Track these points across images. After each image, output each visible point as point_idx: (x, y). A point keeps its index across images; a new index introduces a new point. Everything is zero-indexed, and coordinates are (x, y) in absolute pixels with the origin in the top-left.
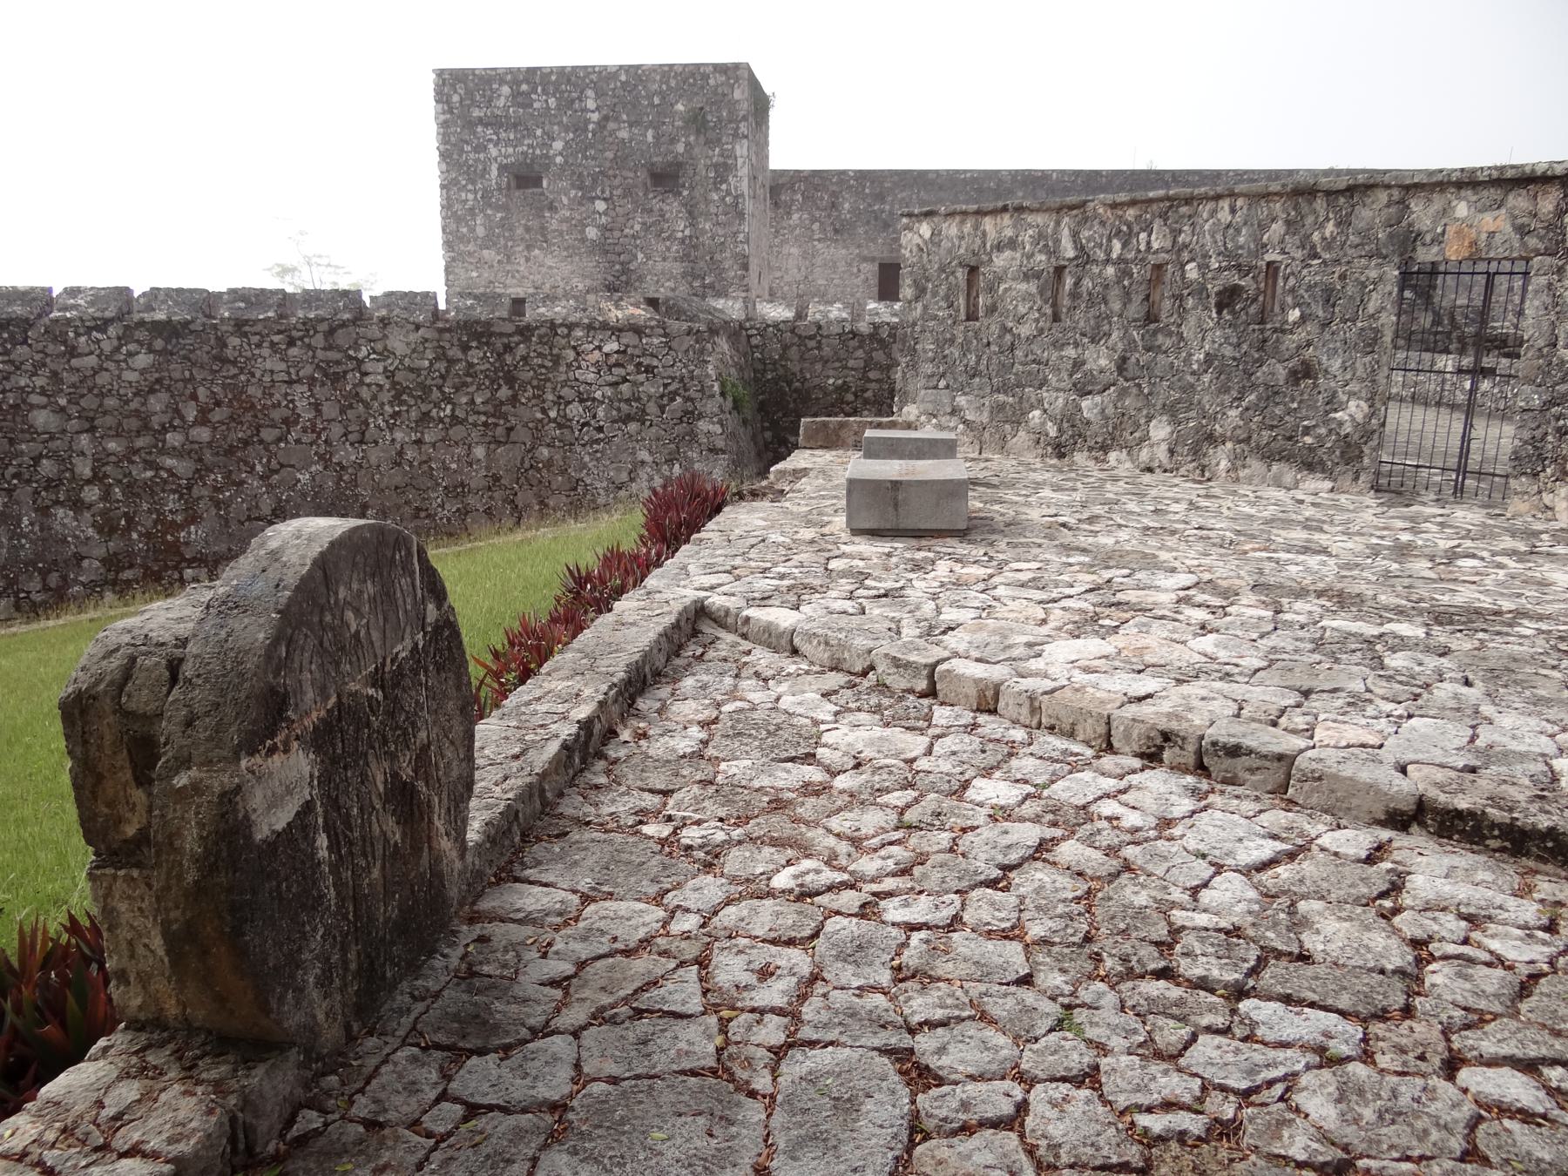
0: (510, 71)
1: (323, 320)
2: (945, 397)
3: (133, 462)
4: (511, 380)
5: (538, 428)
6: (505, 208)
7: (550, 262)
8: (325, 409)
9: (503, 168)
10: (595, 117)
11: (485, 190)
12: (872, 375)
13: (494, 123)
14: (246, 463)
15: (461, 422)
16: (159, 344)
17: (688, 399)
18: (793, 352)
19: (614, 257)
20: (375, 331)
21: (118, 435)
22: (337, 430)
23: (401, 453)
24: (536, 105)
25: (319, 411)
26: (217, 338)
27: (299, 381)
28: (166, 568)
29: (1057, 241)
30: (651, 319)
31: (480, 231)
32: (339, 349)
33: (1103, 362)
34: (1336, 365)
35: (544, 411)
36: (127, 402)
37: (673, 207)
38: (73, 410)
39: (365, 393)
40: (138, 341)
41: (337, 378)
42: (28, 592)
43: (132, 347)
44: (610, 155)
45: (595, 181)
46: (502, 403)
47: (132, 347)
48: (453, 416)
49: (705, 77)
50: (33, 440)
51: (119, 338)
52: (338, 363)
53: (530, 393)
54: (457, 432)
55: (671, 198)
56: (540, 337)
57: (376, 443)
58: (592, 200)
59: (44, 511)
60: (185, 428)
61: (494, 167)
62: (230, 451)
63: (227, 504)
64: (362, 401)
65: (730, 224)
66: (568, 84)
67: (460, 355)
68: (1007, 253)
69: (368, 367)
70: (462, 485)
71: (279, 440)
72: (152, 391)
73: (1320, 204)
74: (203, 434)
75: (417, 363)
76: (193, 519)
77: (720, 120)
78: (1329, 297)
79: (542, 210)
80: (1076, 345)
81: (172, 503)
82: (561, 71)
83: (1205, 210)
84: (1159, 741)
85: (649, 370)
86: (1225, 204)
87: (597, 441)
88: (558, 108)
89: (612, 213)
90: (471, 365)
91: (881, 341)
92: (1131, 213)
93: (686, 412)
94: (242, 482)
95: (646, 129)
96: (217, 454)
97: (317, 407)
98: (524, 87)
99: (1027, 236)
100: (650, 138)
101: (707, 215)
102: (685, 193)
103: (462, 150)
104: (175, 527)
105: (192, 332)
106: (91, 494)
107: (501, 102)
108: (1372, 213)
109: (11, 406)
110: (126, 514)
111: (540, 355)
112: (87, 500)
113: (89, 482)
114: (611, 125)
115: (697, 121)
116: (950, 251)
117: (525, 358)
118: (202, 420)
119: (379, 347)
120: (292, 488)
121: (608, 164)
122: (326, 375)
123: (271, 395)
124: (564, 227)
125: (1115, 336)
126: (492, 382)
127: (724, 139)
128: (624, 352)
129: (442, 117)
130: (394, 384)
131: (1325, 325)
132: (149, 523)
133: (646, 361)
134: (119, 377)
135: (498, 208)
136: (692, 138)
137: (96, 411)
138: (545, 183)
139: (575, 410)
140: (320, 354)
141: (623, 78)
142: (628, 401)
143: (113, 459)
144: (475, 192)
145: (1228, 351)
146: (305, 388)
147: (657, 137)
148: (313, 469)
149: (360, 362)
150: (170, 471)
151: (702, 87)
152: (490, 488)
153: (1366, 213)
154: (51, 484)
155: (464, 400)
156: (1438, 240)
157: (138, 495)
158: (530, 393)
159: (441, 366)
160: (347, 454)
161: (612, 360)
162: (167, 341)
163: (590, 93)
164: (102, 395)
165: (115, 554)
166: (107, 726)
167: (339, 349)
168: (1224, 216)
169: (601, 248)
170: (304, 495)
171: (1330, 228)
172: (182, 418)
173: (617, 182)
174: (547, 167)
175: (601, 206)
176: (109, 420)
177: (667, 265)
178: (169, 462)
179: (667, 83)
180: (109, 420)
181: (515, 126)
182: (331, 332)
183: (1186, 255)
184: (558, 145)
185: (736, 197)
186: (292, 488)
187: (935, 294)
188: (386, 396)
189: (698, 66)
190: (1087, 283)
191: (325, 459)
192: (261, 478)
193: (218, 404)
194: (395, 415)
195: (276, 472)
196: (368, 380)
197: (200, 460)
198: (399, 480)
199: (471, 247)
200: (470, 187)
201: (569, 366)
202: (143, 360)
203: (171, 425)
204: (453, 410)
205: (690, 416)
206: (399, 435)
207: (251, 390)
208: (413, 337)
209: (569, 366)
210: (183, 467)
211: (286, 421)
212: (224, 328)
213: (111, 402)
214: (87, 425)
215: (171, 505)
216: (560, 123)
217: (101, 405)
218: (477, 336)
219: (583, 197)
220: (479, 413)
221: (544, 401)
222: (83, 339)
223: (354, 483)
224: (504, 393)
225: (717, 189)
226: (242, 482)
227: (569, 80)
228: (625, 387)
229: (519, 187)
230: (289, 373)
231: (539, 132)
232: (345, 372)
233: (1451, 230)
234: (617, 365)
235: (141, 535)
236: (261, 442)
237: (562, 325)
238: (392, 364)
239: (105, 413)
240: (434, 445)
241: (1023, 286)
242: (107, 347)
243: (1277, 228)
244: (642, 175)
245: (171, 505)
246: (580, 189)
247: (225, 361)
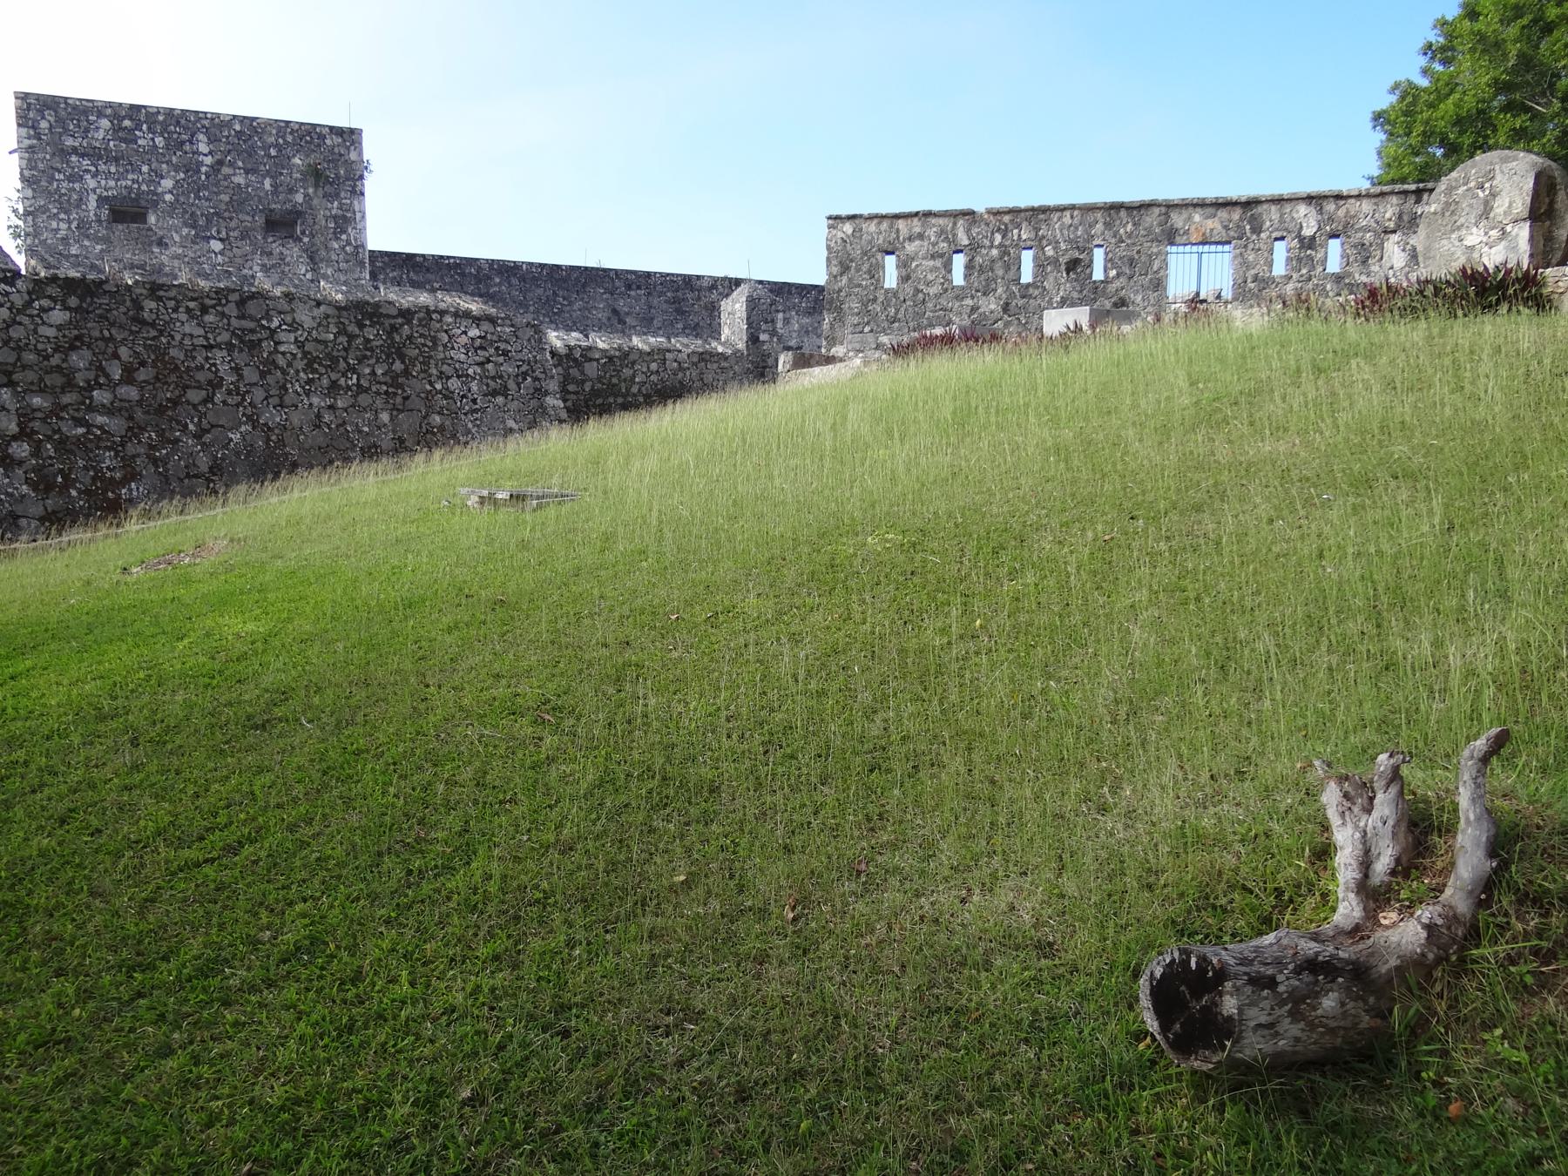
0: (110, 105)
1: (234, 291)
2: (870, 338)
3: (62, 419)
4: (402, 357)
5: (429, 396)
6: (106, 240)
8: (246, 372)
9: (102, 200)
10: (208, 160)
12: (571, 388)
13: (93, 154)
14: (178, 422)
15: (367, 390)
16: (73, 301)
17: (536, 379)
21: (41, 391)
22: (259, 394)
23: (319, 416)
25: (241, 377)
27: (218, 346)
29: (955, 235)
32: (252, 318)
33: (993, 307)
34: (1139, 298)
35: (431, 383)
36: (47, 358)
37: (293, 252)
39: (281, 362)
40: (50, 297)
41: (254, 346)
43: (45, 303)
44: (225, 198)
45: (209, 221)
46: (398, 376)
48: (358, 385)
49: (322, 137)
51: (29, 293)
52: (252, 331)
53: (418, 368)
54: (364, 400)
55: (291, 244)
56: (420, 320)
60: (112, 386)
61: (93, 199)
62: (161, 410)
63: (165, 461)
65: (353, 271)
66: (179, 126)
67: (357, 331)
68: (917, 242)
69: (282, 336)
70: (376, 447)
71: (205, 401)
72: (73, 348)
73: (1123, 213)
74: (132, 393)
75: (324, 336)
77: (337, 176)
78: (1132, 262)
80: (973, 297)
81: (108, 460)
82: (170, 112)
83: (1055, 216)
85: (505, 353)
86: (1068, 213)
88: (167, 147)
89: (228, 253)
90: (368, 341)
91: (575, 360)
92: (1006, 218)
93: (536, 390)
96: (148, 413)
97: (237, 370)
98: (127, 123)
99: (931, 233)
101: (329, 261)
102: (306, 240)
103: (53, 178)
104: (115, 484)
105: (105, 292)
106: (21, 450)
107: (100, 135)
108: (1152, 218)
110: (61, 471)
111: (422, 335)
112: (17, 456)
113: (15, 438)
114: (226, 170)
115: (316, 175)
116: (870, 242)
117: (410, 337)
118: (128, 377)
119: (289, 319)
120: (226, 446)
121: (224, 207)
122: (242, 341)
125: (1000, 291)
126: (388, 356)
127: (343, 194)
129: (27, 142)
130: (305, 354)
131: (1131, 278)
132: (88, 481)
133: (502, 346)
134: (35, 331)
135: (97, 240)
136: (311, 190)
139: (454, 384)
140: (234, 322)
141: (238, 127)
142: (493, 378)
143: (39, 415)
144: (69, 222)
145: (1075, 295)
146: (225, 353)
147: (275, 186)
148: (243, 429)
149: (273, 332)
150: (101, 428)
151: (319, 146)
153: (1148, 219)
155: (367, 371)
156: (1187, 232)
157: (71, 452)
158: (418, 368)
159: (343, 339)
160: (271, 416)
161: (478, 342)
162: (82, 300)
165: (54, 512)
166: (1543, 180)
167: (252, 318)
168: (1067, 220)
170: (238, 454)
171: (1129, 227)
172: (107, 376)
173: (233, 224)
174: (155, 204)
175: (216, 246)
176: (31, 376)
178: (100, 419)
179: (283, 138)
180: (31, 376)
182: (241, 303)
183: (1045, 242)
184: (167, 183)
185: (356, 247)
186: (226, 446)
187: (858, 270)
188: (300, 365)
189: (314, 126)
190: (979, 260)
191: (253, 420)
192: (195, 436)
193: (143, 364)
194: (309, 382)
195: (208, 431)
196: (282, 349)
197: (131, 418)
198: (321, 441)
200: (62, 216)
201: (445, 346)
202: (58, 316)
203: (97, 383)
205: (539, 392)
206: (315, 400)
207: (173, 352)
208: (316, 312)
209: (445, 346)
210: (116, 425)
211: (210, 382)
212: (138, 291)
213: (30, 357)
215: (108, 462)
217: (19, 359)
218: (371, 316)
219: (197, 235)
223: (281, 442)
224: (398, 366)
225: (337, 239)
226: (177, 441)
227: (178, 123)
228: (490, 366)
230: (207, 339)
231: (145, 169)
232: (260, 340)
233: (1193, 228)
234: (482, 348)
235: (80, 492)
236: (188, 402)
239: (24, 367)
240: (346, 410)
241: (931, 263)
242: (18, 301)
243: (1100, 226)
244: (260, 220)
245: (108, 462)
246: (194, 227)
247: (143, 322)
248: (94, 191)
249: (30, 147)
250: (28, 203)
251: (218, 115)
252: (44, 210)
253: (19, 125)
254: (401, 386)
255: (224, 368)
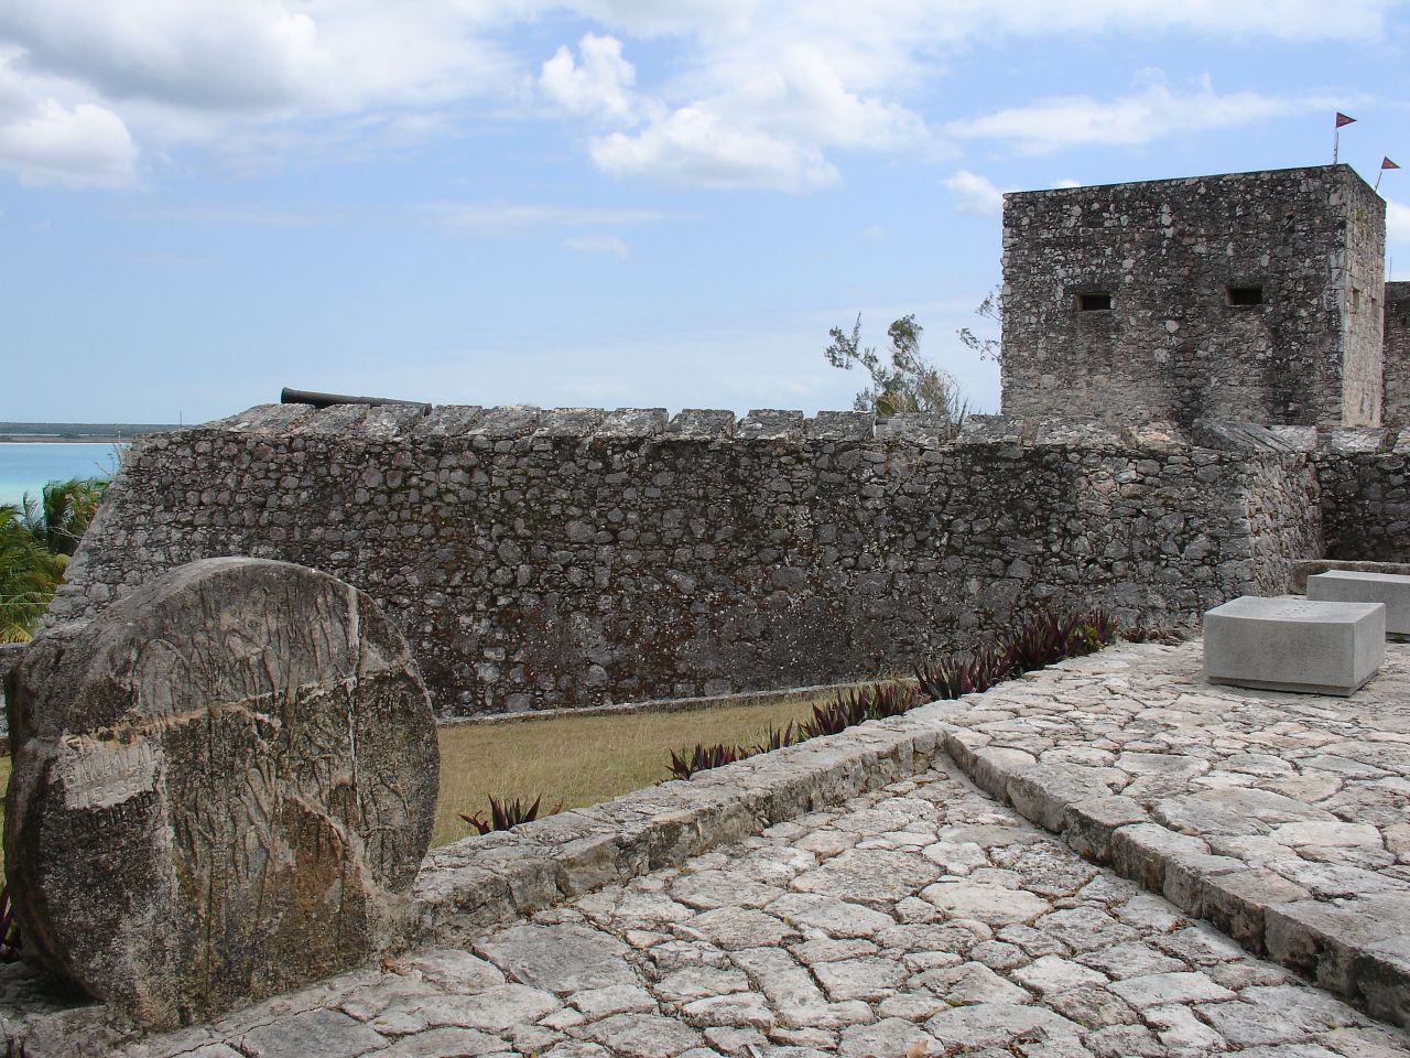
7: (1115, 386)
9: (1068, 291)
10: (1170, 232)
11: (1049, 314)
13: (1061, 243)
15: (957, 552)
18: (1374, 490)
19: (1187, 383)
20: (879, 456)
23: (892, 582)
24: (1106, 224)
26: (732, 458)
28: (660, 680)
30: (1175, 446)
31: (1042, 355)
38: (602, 523)
42: (543, 691)
47: (658, 465)
50: (566, 548)
54: (953, 563)
55: (1252, 317)
57: (868, 569)
58: (1163, 320)
59: (565, 615)
61: (1060, 288)
62: (731, 568)
64: (858, 524)
74: (708, 551)
76: (689, 634)
79: (1107, 331)
84: (1311, 949)
87: (1103, 581)
88: (1131, 225)
89: (1183, 333)
94: (736, 602)
95: (1227, 242)
100: (1230, 252)
103: (1028, 272)
106: (605, 602)
109: (553, 517)
113: (605, 591)
123: (773, 516)
124: (1131, 349)
128: (1141, 482)
135: (1060, 331)
137: (620, 524)
138: (1112, 303)
141: (1202, 190)
144: (1039, 315)
149: (861, 485)
152: (980, 627)
154: (576, 591)
163: (1165, 208)
164: (625, 510)
169: (1169, 372)
175: (1172, 326)
177: (1245, 390)
180: (629, 534)
181: (1084, 245)
184: (1128, 263)
194: (891, 542)
195: (769, 593)
197: (703, 576)
199: (1031, 372)
200: (1034, 310)
204: (949, 539)
210: (688, 583)
214: (611, 538)
216: (1132, 241)
217: (625, 519)
220: (976, 543)
221: (1047, 534)
222: (617, 457)
226: (736, 602)
229: (1085, 308)
231: (1108, 251)
235: (642, 646)
237: (1073, 450)
238: (893, 488)
239: (627, 526)
248: (1062, 280)
249: (1014, 245)
250: (1006, 301)
251: (1183, 180)
252: (1020, 305)
253: (1005, 225)
254: (1002, 547)
255: (801, 527)
